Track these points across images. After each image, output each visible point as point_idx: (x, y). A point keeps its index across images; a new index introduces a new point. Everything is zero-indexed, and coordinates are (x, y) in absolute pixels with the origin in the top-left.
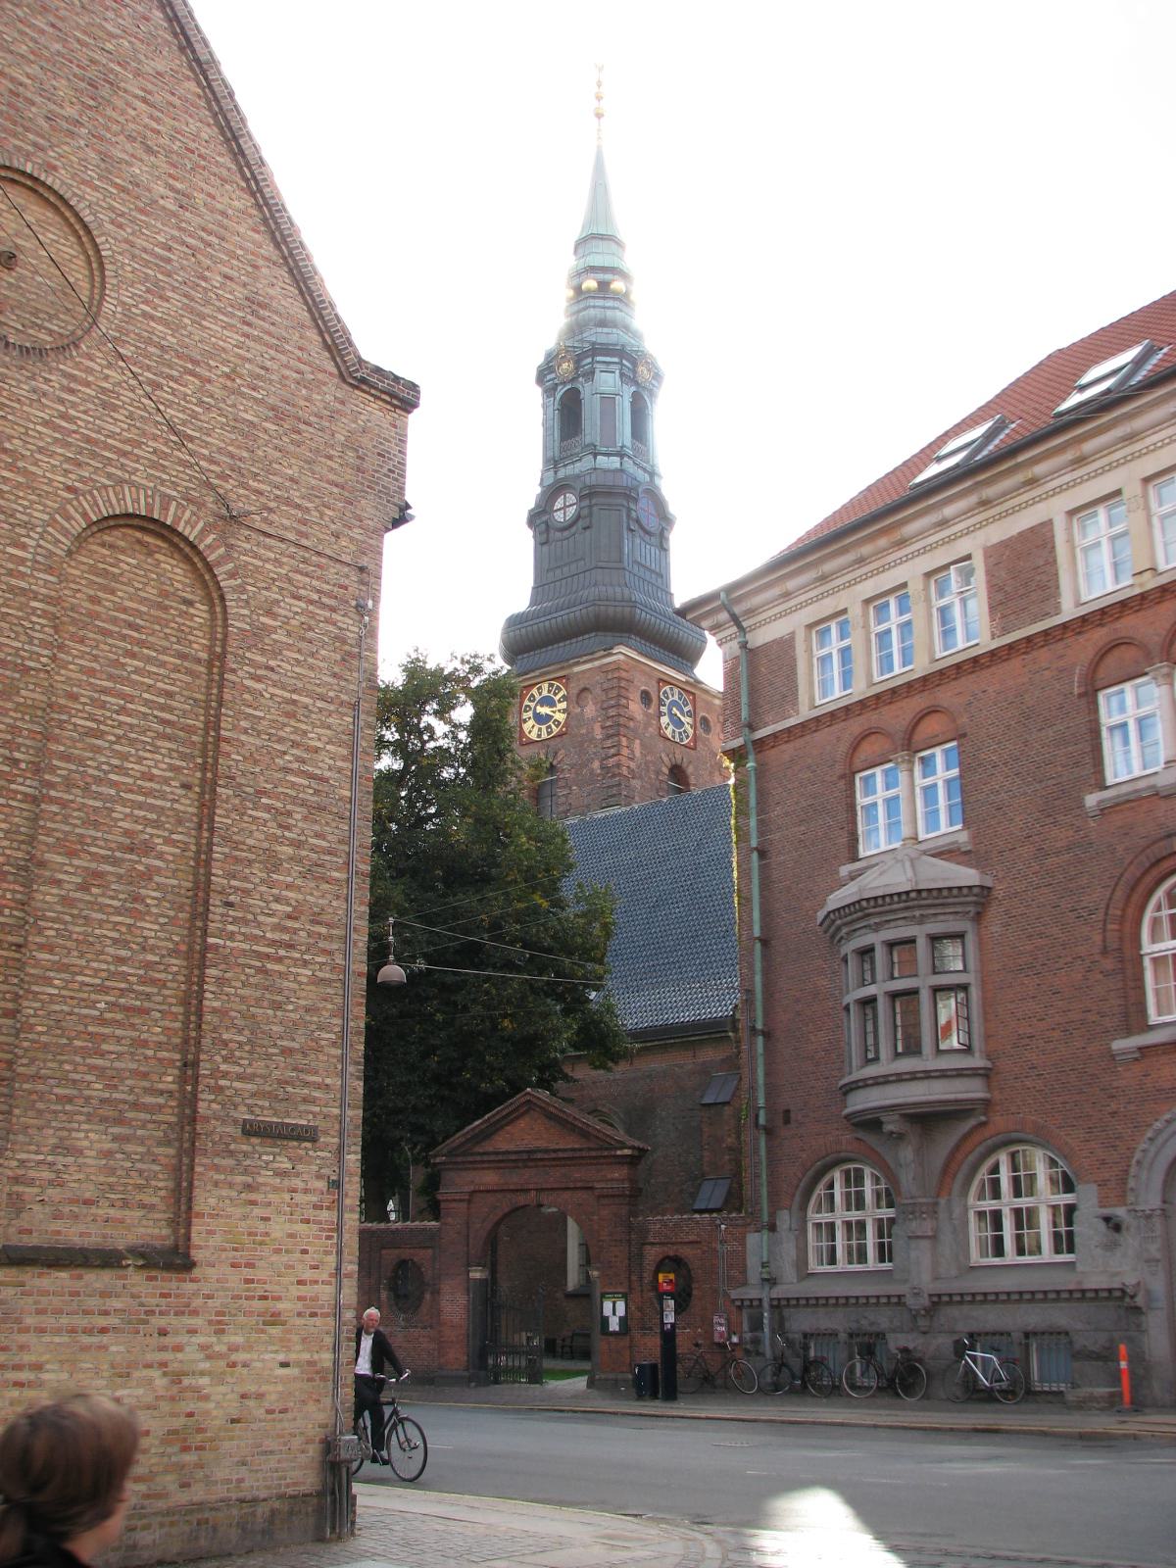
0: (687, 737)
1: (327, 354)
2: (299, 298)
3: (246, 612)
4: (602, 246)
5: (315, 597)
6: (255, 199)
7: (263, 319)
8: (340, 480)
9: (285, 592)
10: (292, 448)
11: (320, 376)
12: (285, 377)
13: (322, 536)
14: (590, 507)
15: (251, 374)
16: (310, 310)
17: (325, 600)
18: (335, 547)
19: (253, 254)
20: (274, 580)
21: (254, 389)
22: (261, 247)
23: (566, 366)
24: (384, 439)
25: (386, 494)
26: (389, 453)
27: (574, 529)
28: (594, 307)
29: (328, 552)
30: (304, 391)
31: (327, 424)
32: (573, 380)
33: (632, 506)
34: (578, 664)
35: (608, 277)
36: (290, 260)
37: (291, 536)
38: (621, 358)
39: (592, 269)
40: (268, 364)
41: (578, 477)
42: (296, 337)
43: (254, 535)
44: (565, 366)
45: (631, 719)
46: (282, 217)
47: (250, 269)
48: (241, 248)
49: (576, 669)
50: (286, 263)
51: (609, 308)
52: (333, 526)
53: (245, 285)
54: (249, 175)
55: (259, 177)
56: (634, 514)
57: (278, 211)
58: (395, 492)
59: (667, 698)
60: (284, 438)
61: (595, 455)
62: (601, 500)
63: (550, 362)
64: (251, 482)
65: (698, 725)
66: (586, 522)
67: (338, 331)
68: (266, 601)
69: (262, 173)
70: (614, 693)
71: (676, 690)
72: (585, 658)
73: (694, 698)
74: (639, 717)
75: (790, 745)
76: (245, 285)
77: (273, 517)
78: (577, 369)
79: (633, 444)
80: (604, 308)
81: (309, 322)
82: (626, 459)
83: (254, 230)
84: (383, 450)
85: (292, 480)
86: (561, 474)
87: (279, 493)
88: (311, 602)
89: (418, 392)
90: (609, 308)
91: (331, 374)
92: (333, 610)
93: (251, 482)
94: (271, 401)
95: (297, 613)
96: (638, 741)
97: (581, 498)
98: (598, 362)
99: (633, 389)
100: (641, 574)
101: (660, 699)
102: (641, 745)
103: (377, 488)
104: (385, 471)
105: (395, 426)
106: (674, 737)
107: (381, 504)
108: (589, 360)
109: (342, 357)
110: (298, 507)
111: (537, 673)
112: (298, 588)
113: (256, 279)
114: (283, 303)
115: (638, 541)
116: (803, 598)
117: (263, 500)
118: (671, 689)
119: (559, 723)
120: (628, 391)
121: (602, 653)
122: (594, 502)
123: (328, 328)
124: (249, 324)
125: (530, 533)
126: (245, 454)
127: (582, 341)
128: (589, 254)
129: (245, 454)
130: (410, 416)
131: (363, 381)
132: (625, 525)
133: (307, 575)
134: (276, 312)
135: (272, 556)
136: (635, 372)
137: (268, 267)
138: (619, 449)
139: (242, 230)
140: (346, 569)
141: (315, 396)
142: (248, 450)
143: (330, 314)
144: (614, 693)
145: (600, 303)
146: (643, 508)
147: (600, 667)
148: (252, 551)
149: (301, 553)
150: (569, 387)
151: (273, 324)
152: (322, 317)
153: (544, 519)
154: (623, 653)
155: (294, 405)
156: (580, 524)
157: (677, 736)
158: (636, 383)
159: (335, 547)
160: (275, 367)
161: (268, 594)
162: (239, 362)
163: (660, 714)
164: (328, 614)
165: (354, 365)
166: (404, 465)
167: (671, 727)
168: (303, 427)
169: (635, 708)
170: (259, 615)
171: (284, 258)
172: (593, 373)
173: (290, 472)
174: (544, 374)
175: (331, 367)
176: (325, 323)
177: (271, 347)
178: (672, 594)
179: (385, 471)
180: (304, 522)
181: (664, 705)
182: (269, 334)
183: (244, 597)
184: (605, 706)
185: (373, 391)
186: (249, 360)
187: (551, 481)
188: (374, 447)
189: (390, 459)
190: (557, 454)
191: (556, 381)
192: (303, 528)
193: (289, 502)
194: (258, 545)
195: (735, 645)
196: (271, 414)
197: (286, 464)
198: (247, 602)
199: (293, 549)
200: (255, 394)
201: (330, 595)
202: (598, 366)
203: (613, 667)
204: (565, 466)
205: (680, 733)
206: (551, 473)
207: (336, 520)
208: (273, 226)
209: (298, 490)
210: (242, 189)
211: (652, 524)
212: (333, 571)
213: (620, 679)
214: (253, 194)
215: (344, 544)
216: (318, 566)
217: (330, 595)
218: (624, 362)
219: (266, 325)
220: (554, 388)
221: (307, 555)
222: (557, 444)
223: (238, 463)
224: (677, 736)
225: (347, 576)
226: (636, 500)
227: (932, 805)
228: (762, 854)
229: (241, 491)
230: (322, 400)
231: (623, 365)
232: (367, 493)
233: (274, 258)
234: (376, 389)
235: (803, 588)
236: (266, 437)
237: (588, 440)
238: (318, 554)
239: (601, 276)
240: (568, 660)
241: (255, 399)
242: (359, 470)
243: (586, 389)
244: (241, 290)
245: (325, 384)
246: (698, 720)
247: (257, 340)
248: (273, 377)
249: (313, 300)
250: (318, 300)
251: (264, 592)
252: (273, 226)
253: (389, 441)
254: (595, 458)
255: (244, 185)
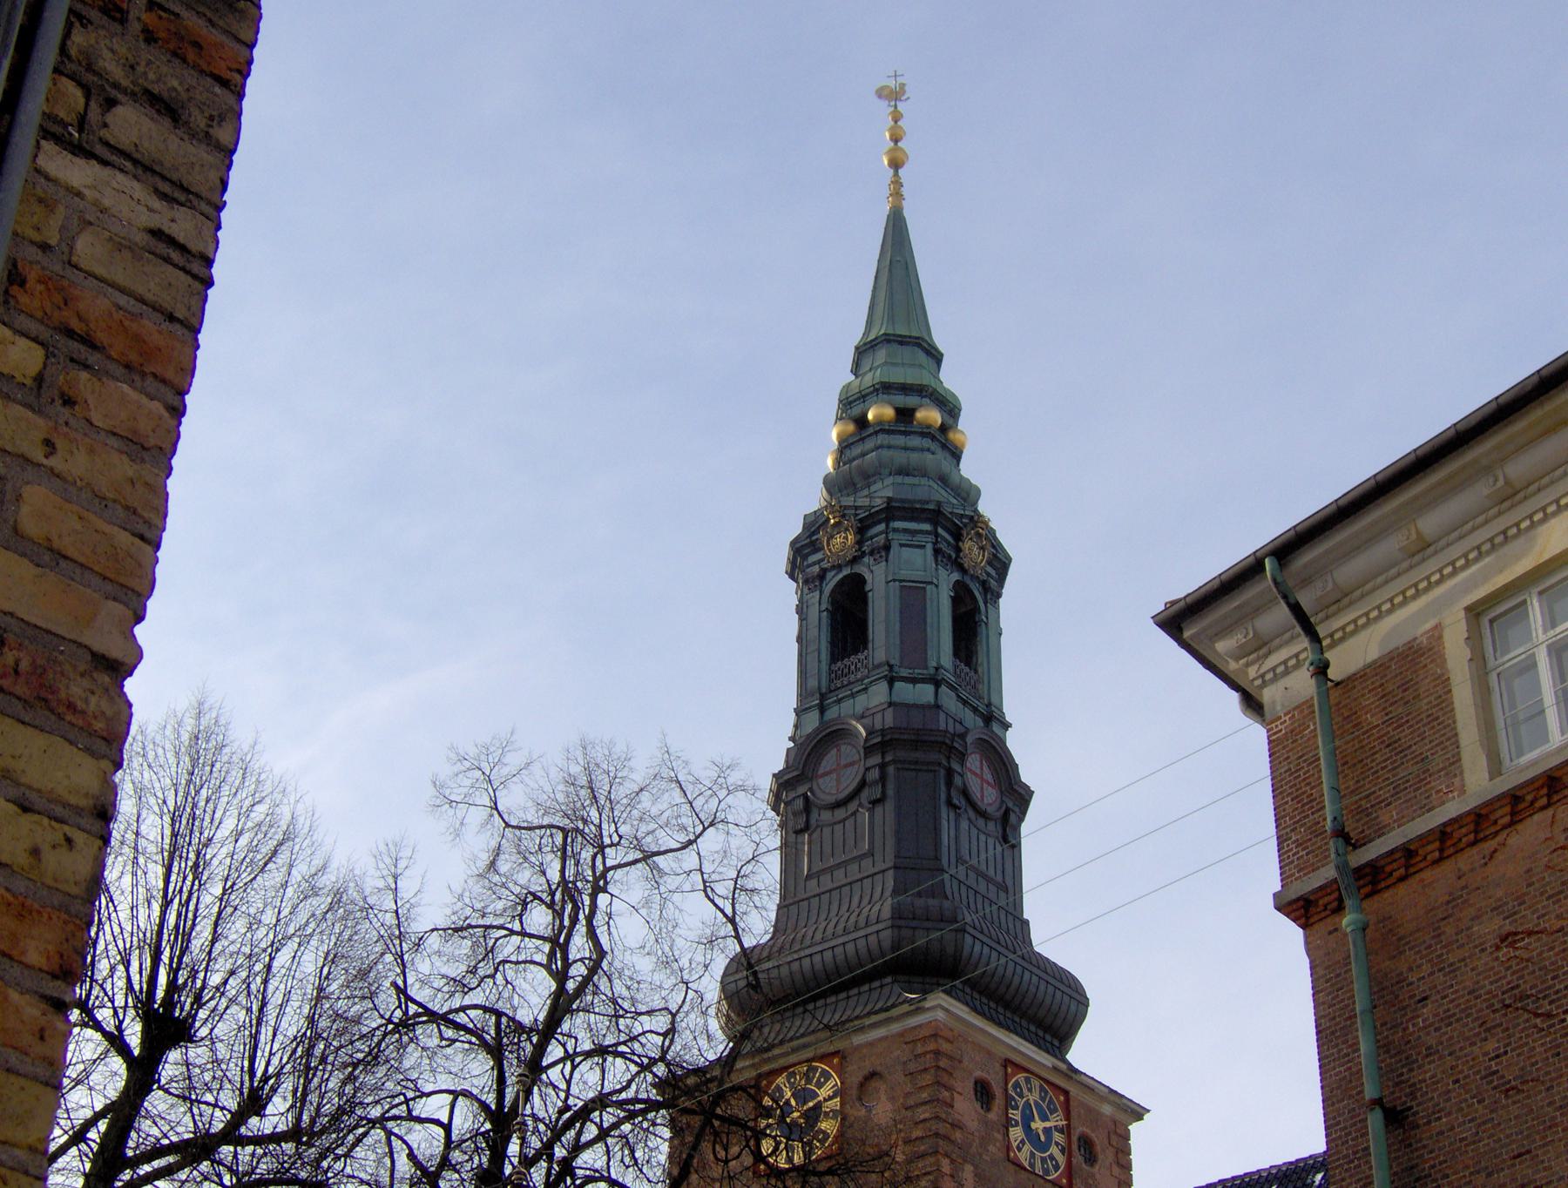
0: (1057, 1167)
23: (843, 541)
27: (852, 806)
28: (889, 447)
32: (855, 560)
33: (956, 766)
35: (911, 401)
38: (935, 524)
45: (956, 1126)
49: (858, 1039)
51: (913, 449)
56: (958, 781)
59: (1021, 1096)
61: (891, 681)
63: (814, 533)
65: (1075, 1147)
66: (877, 792)
70: (928, 1078)
71: (1036, 1083)
73: (1067, 1100)
74: (972, 1124)
75: (1447, 867)
78: (860, 543)
79: (956, 667)
80: (906, 449)
82: (943, 688)
90: (913, 449)
96: (969, 1168)
98: (895, 530)
99: (956, 576)
100: (971, 881)
101: (1008, 1098)
102: (977, 1176)
106: (1032, 1165)
108: (882, 527)
115: (964, 825)
118: (1027, 1080)
119: (827, 1136)
120: (947, 579)
122: (888, 758)
132: (943, 796)
136: (958, 550)
138: (932, 671)
144: (928, 1078)
145: (900, 440)
146: (976, 774)
147: (902, 1034)
150: (846, 571)
153: (801, 790)
154: (943, 1008)
156: (865, 794)
157: (1038, 1164)
158: (962, 569)
163: (1008, 1123)
167: (1027, 1147)
169: (965, 1107)
172: (887, 548)
174: (803, 551)
178: (1027, 923)
181: (1016, 1108)
184: (911, 1102)
190: (824, 683)
191: (825, 565)
203: (925, 1032)
205: (1043, 1160)
206: (815, 715)
211: (988, 797)
213: (937, 1053)
218: (940, 530)
220: (822, 576)
222: (824, 667)
224: (1038, 1164)
226: (962, 757)
228: (1395, 1118)
231: (937, 535)
235: (1457, 529)
246: (1075, 1139)
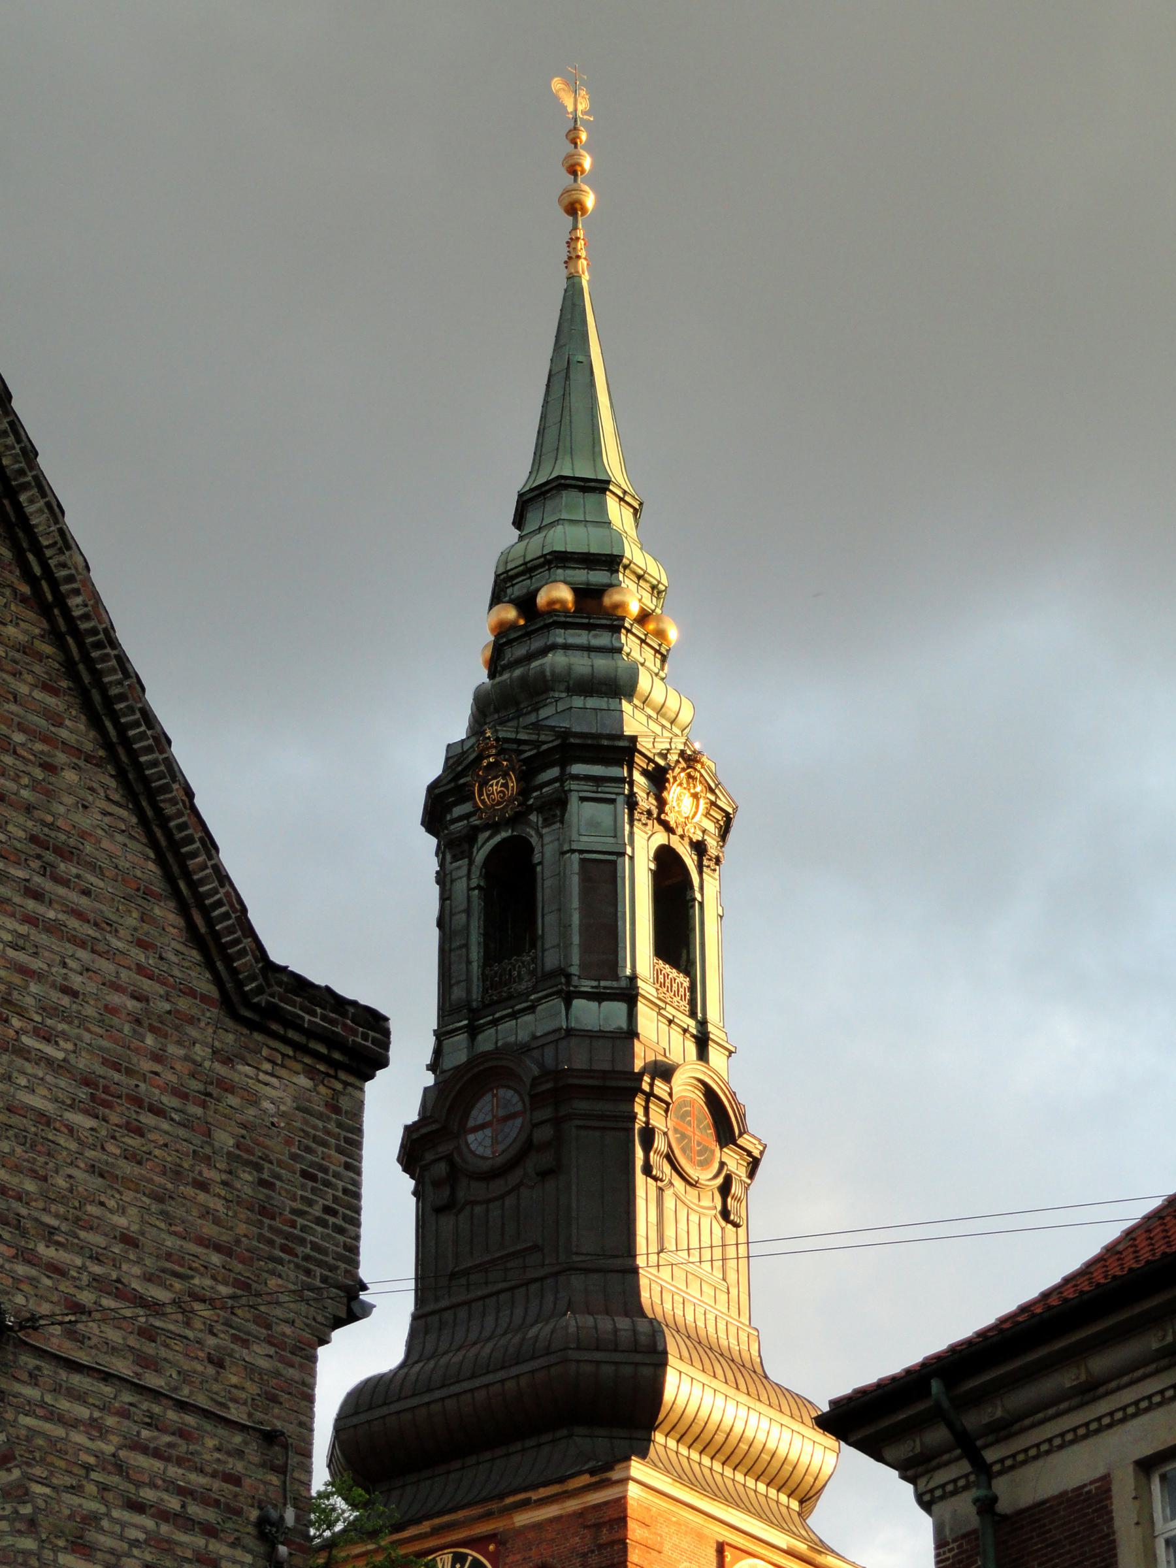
1: (195, 955)
2: (138, 832)
3: (29, 1544)
4: (571, 503)
5: (173, 1503)
6: (51, 619)
7: (65, 882)
8: (226, 1238)
9: (110, 1496)
10: (127, 1168)
11: (183, 1004)
12: (112, 1010)
13: (187, 1365)
14: (557, 1122)
15: (46, 1009)
16: (161, 860)
17: (194, 1510)
18: (216, 1387)
19: (45, 740)
20: (88, 1468)
21: (47, 1040)
22: (60, 725)
24: (315, 1139)
25: (320, 1264)
26: (325, 1170)
28: (566, 647)
29: (202, 1401)
30: (150, 1040)
31: (199, 1111)
32: (519, 818)
34: (525, 1504)
36: (121, 750)
37: (123, 1367)
39: (559, 560)
40: (76, 981)
41: (524, 1049)
42: (132, 921)
43: (47, 1368)
44: (495, 787)
46: (105, 658)
47: (38, 773)
48: (21, 728)
49: (522, 1519)
50: (113, 757)
52: (211, 1341)
53: (29, 809)
54: (37, 570)
55: (61, 574)
57: (99, 645)
58: (339, 1257)
60: (111, 1148)
62: (582, 1106)
64: (41, 1248)
67: (219, 903)
68: (71, 1517)
69: (64, 565)
72: (543, 1492)
76: (29, 809)
77: (91, 1328)
78: (524, 792)
81: (158, 886)
83: (46, 687)
84: (312, 1164)
85: (127, 1240)
86: (487, 1041)
87: (97, 1269)
88: (164, 1515)
89: (387, 1033)
91: (204, 998)
92: (210, 1531)
93: (41, 1248)
94: (83, 1062)
95: (135, 1543)
97: (536, 1100)
98: (576, 777)
103: (300, 1250)
104: (316, 1211)
105: (337, 1110)
107: (311, 1289)
108: (554, 772)
109: (228, 960)
110: (140, 1301)
111: (426, 1527)
112: (138, 1485)
113: (49, 794)
114: (105, 844)
116: (1128, 1396)
117: (65, 1286)
121: (585, 1479)
123: (199, 898)
124: (37, 895)
125: (408, 1183)
126: (30, 1186)
127: (537, 727)
128: (552, 524)
129: (30, 1186)
130: (369, 1086)
131: (273, 1012)
133: (157, 1454)
134: (93, 867)
135: (83, 1412)
137: (75, 767)
138: (624, 983)
139: (24, 689)
140: (238, 1439)
141: (172, 1049)
142: (35, 1175)
143: (204, 867)
145: (580, 637)
148: (43, 1404)
149: (145, 1406)
151: (86, 893)
152: (187, 874)
153: (444, 1149)
155: (129, 1072)
159: (216, 1387)
160: (92, 987)
161: (75, 1500)
162: (17, 979)
164: (200, 1541)
165: (253, 978)
166: (357, 1196)
168: (148, 1119)
170: (55, 1549)
171: (108, 745)
173: (122, 1221)
175: (203, 984)
176: (193, 885)
177: (82, 944)
179: (316, 1211)
180: (148, 1334)
182: (79, 915)
183: (26, 1510)
185: (291, 1034)
186: (38, 976)
187: (461, 1057)
188: (294, 1157)
189: (327, 1184)
190: (476, 994)
191: (475, 821)
192: (150, 1349)
193: (119, 1290)
194: (56, 1390)
195: (964, 1506)
196: (83, 1093)
197: (111, 1203)
198: (32, 1523)
199: (127, 1397)
200: (49, 1050)
201: (205, 1500)
202: (574, 785)
204: (495, 1023)
207: (218, 1327)
208: (87, 679)
209: (139, 1262)
210: (24, 600)
212: (210, 1443)
214: (45, 610)
215: (234, 1380)
216: (182, 1433)
217: (205, 1500)
219: (74, 897)
220: (471, 836)
221: (157, 1409)
223: (15, 1205)
225: (239, 1454)
227: (53, 849)
229: (21, 1269)
230: (186, 1058)
232: (280, 1261)
233: (88, 747)
234: (299, 1028)
236: (73, 1146)
237: (551, 960)
238: (182, 1406)
239: (582, 576)
240: (502, 1496)
241: (49, 1062)
242: (263, 1211)
243: (545, 846)
244: (21, 819)
245: (192, 1021)
247: (53, 928)
248: (89, 1011)
249: (169, 834)
250: (179, 836)
251: (66, 1497)
252: (87, 679)
253: (324, 1144)
254: (568, 1006)
255: (25, 589)
